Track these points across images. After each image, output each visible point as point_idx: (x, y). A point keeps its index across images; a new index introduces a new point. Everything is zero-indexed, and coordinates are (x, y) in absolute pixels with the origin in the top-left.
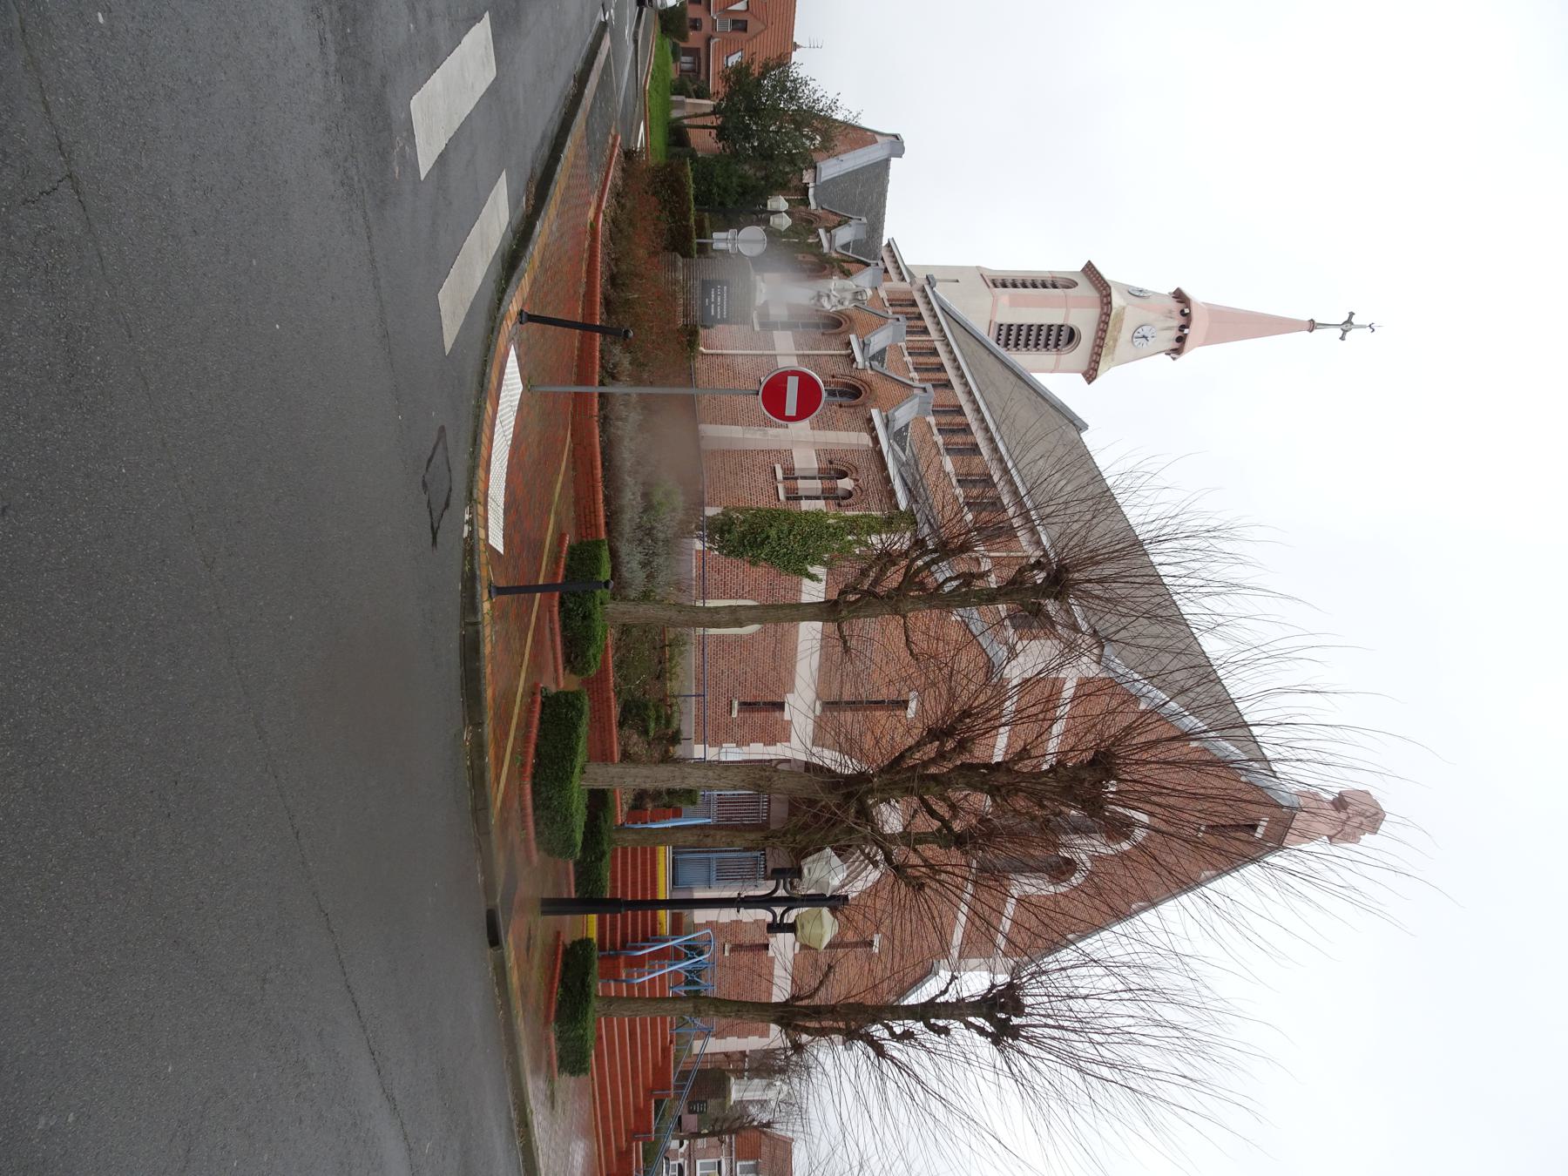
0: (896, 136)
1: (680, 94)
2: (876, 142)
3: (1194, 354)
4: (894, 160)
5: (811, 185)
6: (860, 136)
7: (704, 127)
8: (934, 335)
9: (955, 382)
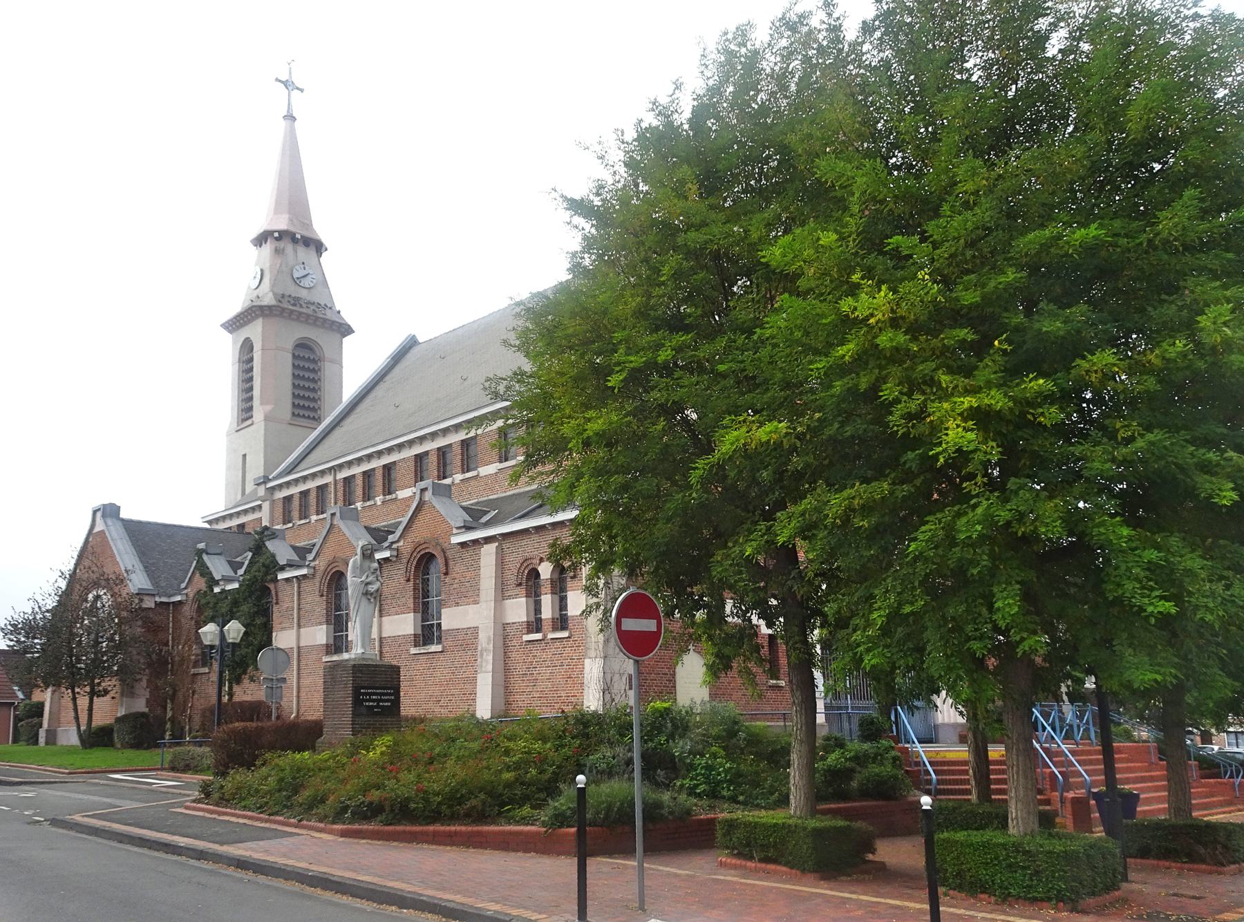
0: (95, 512)
1: (36, 736)
2: (102, 532)
3: (322, 229)
4: (123, 515)
5: (157, 599)
6: (93, 549)
7: (90, 709)
8: (328, 479)
9: (386, 460)
